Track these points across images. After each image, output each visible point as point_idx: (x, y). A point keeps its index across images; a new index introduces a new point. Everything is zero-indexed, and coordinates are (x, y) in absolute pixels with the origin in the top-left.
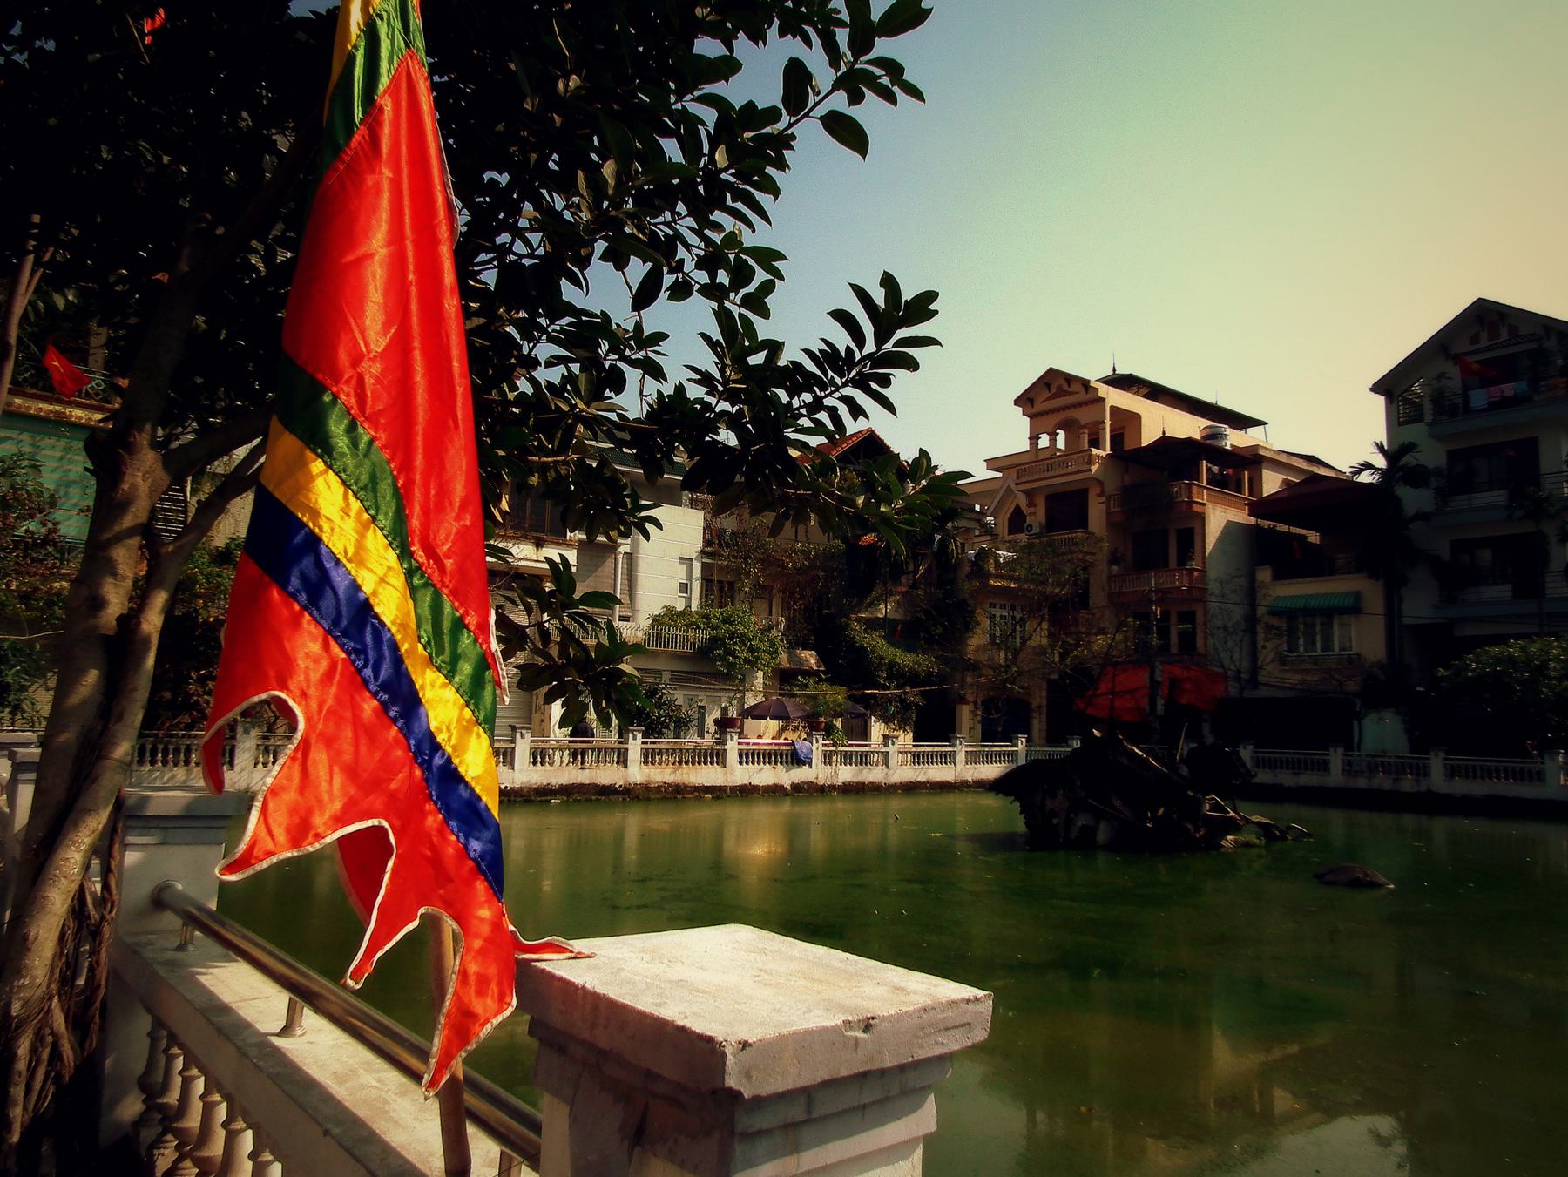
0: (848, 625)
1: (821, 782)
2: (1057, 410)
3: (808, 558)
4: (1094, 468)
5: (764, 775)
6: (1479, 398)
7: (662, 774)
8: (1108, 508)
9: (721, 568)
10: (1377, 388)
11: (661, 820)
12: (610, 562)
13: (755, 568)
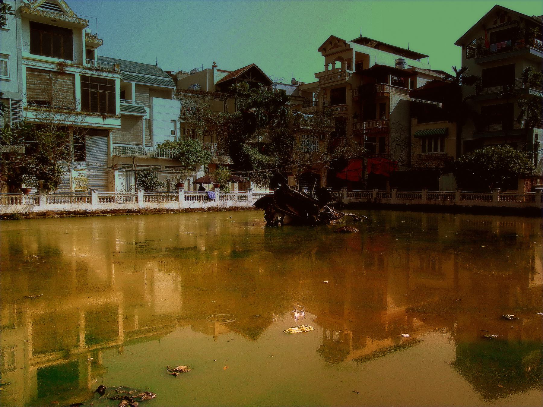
1: (219, 207)
2: (337, 53)
4: (347, 79)
6: (494, 48)
7: (153, 205)
8: (353, 95)
9: (188, 124)
10: (458, 43)
11: (153, 221)
12: (140, 122)
13: (202, 123)
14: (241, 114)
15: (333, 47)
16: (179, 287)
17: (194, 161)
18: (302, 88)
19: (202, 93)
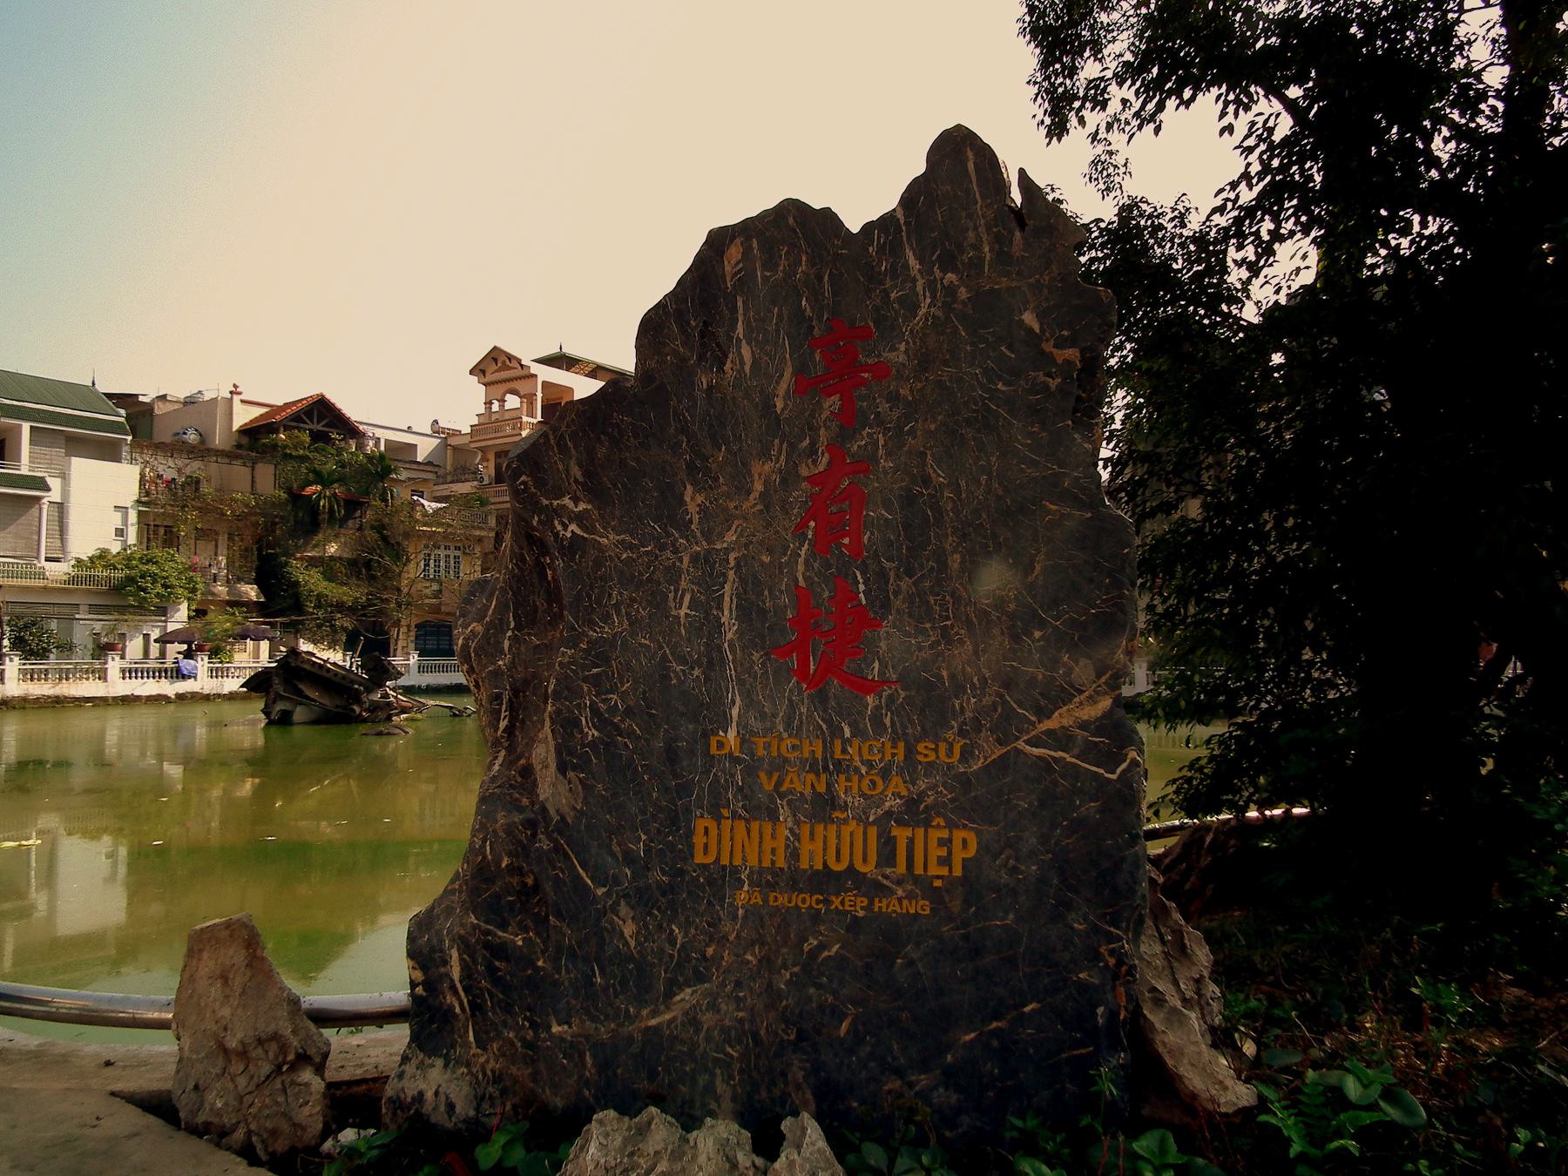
0: (286, 564)
1: (206, 692)
3: (247, 506)
5: (149, 687)
9: (157, 515)
11: (44, 725)
14: (284, 496)
15: (497, 368)
16: (122, 870)
17: (158, 595)
18: (453, 441)
19: (201, 451)
